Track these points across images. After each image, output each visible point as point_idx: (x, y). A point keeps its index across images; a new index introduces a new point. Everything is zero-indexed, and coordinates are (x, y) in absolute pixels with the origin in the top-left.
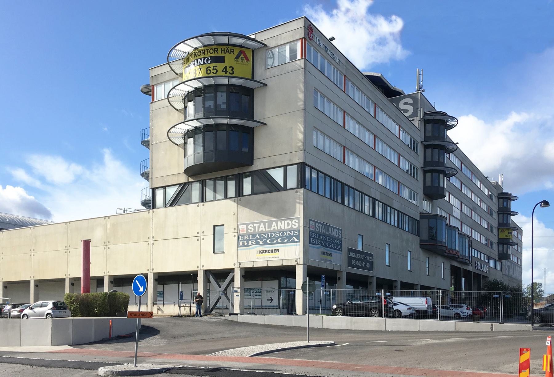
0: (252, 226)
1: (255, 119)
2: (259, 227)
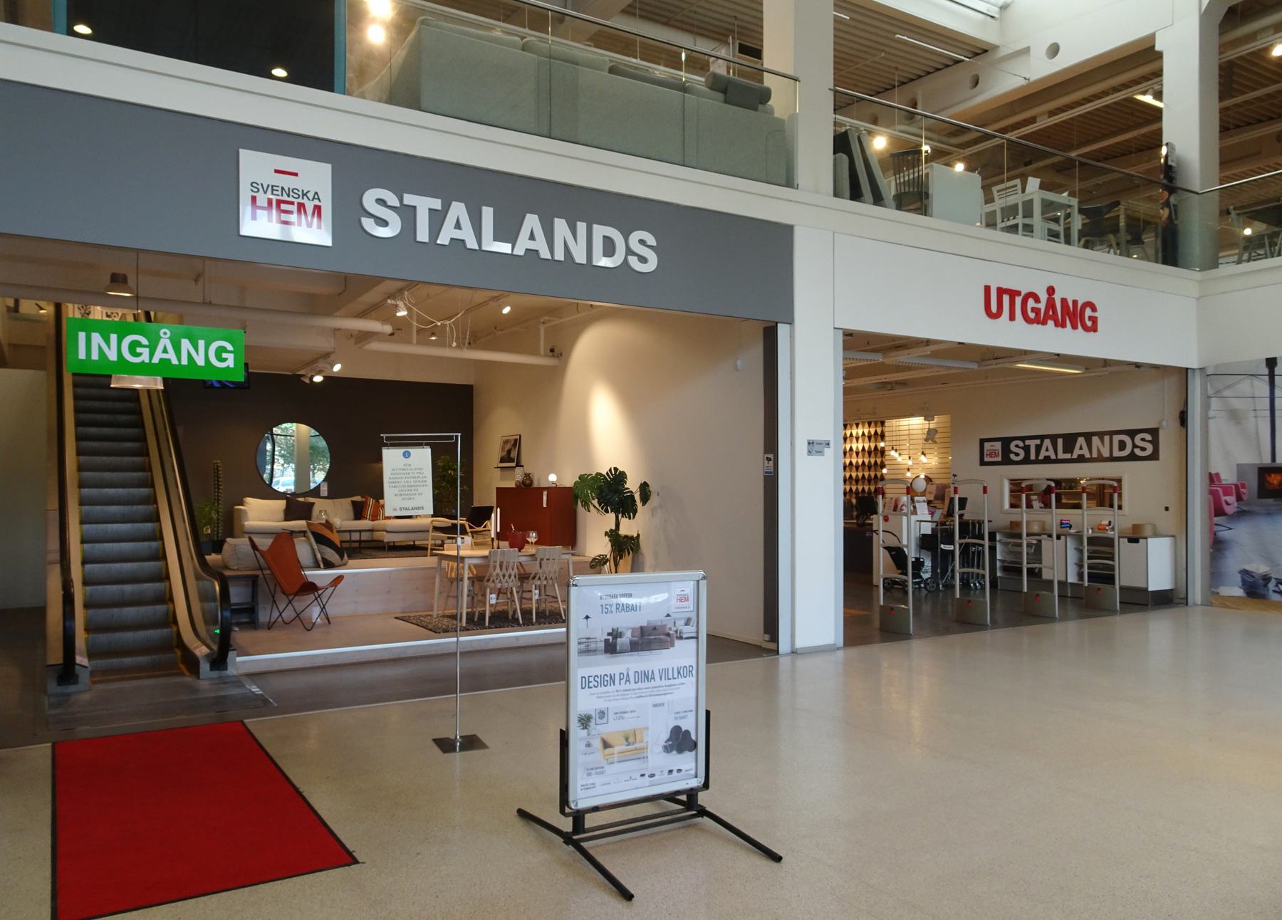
0: (1021, 444)
1: (565, 640)
2: (1038, 448)
